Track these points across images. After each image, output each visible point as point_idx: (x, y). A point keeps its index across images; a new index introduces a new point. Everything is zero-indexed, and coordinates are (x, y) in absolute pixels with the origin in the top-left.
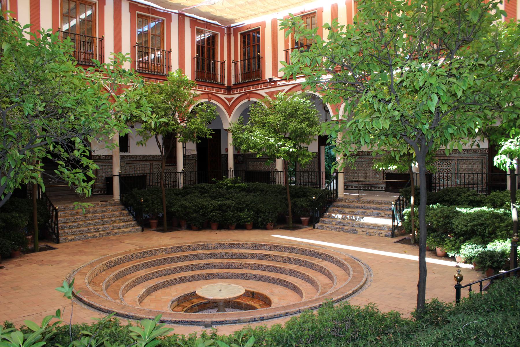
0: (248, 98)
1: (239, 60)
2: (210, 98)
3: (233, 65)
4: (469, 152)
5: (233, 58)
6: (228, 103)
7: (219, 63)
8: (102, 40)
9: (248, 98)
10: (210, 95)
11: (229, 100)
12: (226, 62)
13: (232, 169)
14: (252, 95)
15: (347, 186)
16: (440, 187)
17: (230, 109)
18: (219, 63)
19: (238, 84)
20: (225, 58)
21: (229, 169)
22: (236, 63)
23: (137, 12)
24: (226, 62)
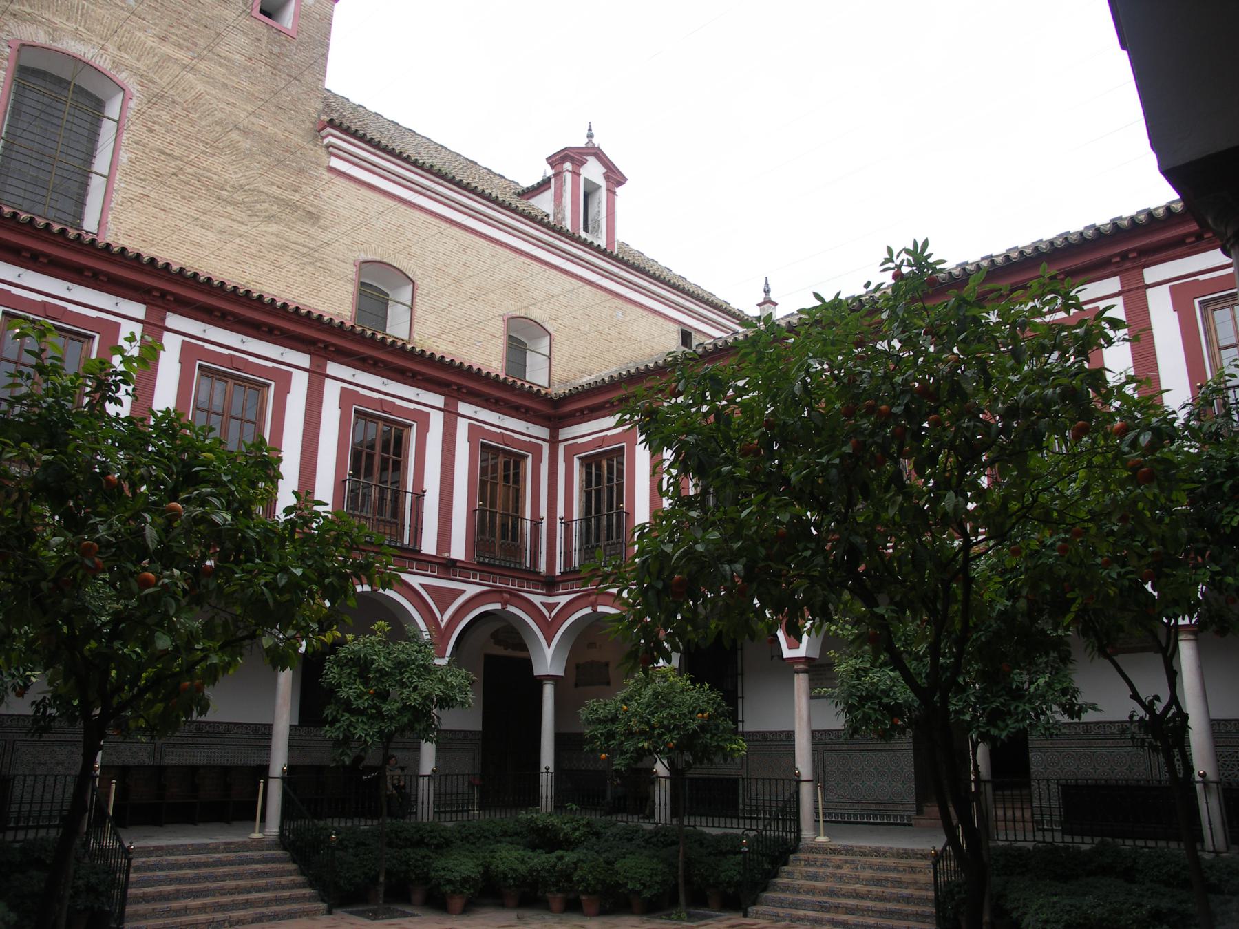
0: (594, 605)
1: (576, 516)
2: (505, 603)
3: (560, 528)
4: (1073, 731)
5: (561, 512)
6: (547, 614)
7: (409, 497)
8: (419, 496)
9: (594, 605)
10: (506, 596)
11: (550, 607)
12: (545, 522)
13: (551, 770)
14: (601, 598)
15: (830, 814)
16: (1051, 815)
17: (549, 628)
18: (409, 497)
19: (570, 572)
20: (543, 513)
21: (543, 770)
22: (568, 524)
23: (198, 362)
24: (545, 522)
